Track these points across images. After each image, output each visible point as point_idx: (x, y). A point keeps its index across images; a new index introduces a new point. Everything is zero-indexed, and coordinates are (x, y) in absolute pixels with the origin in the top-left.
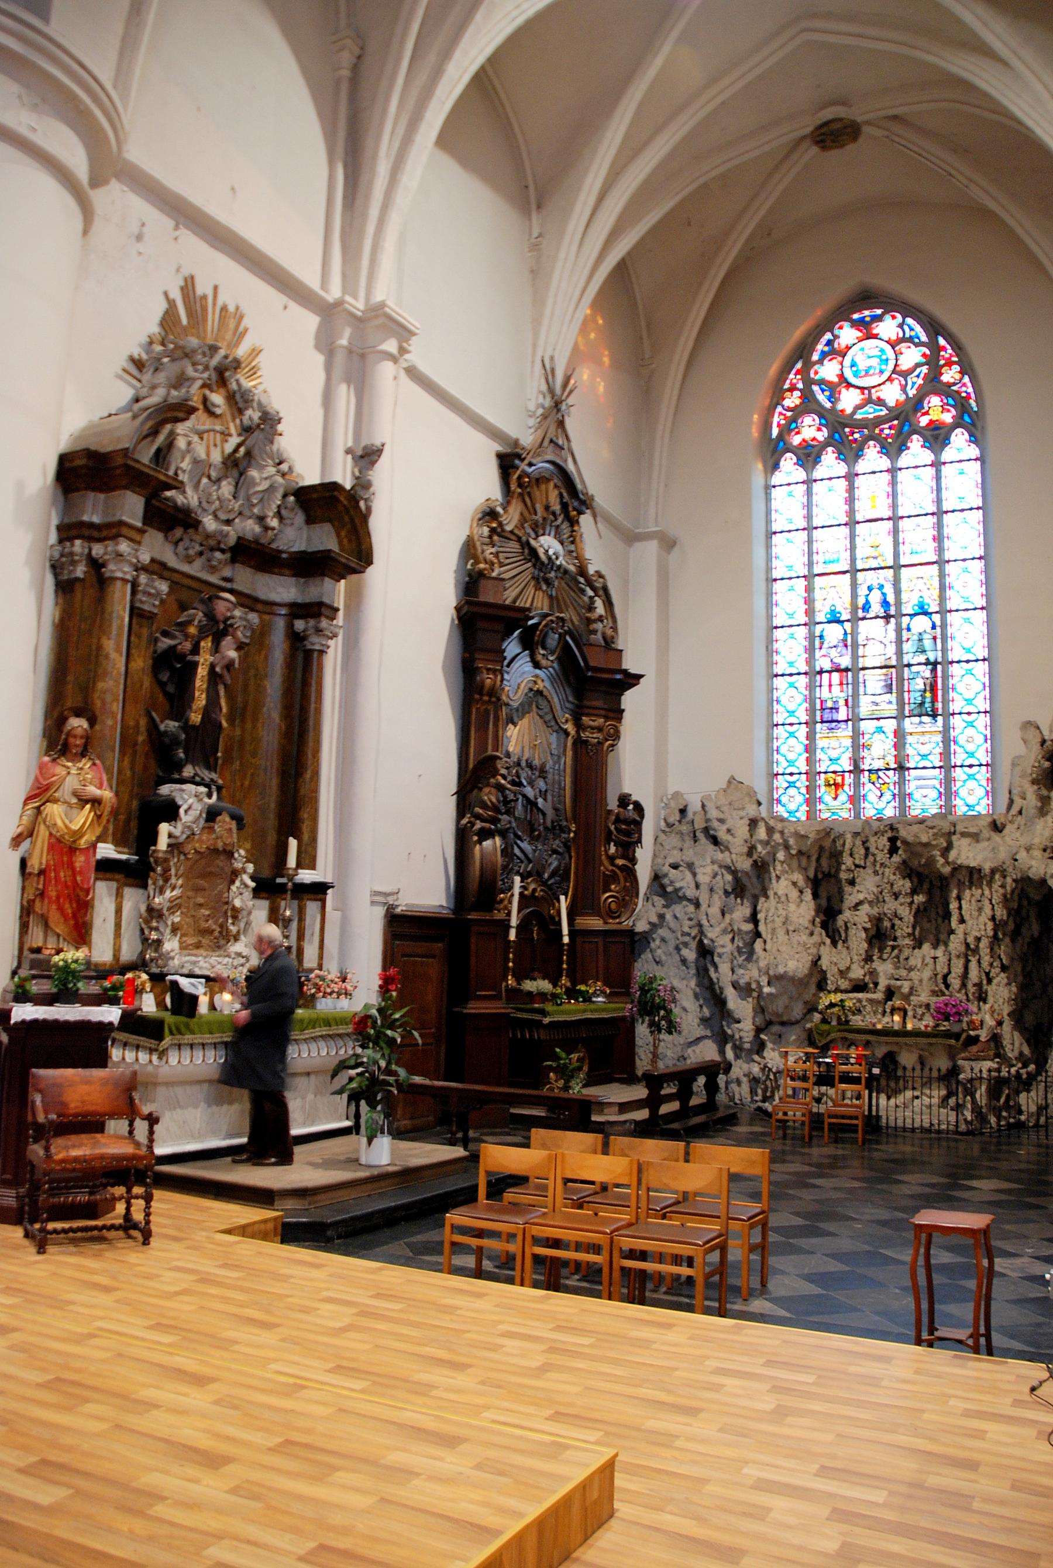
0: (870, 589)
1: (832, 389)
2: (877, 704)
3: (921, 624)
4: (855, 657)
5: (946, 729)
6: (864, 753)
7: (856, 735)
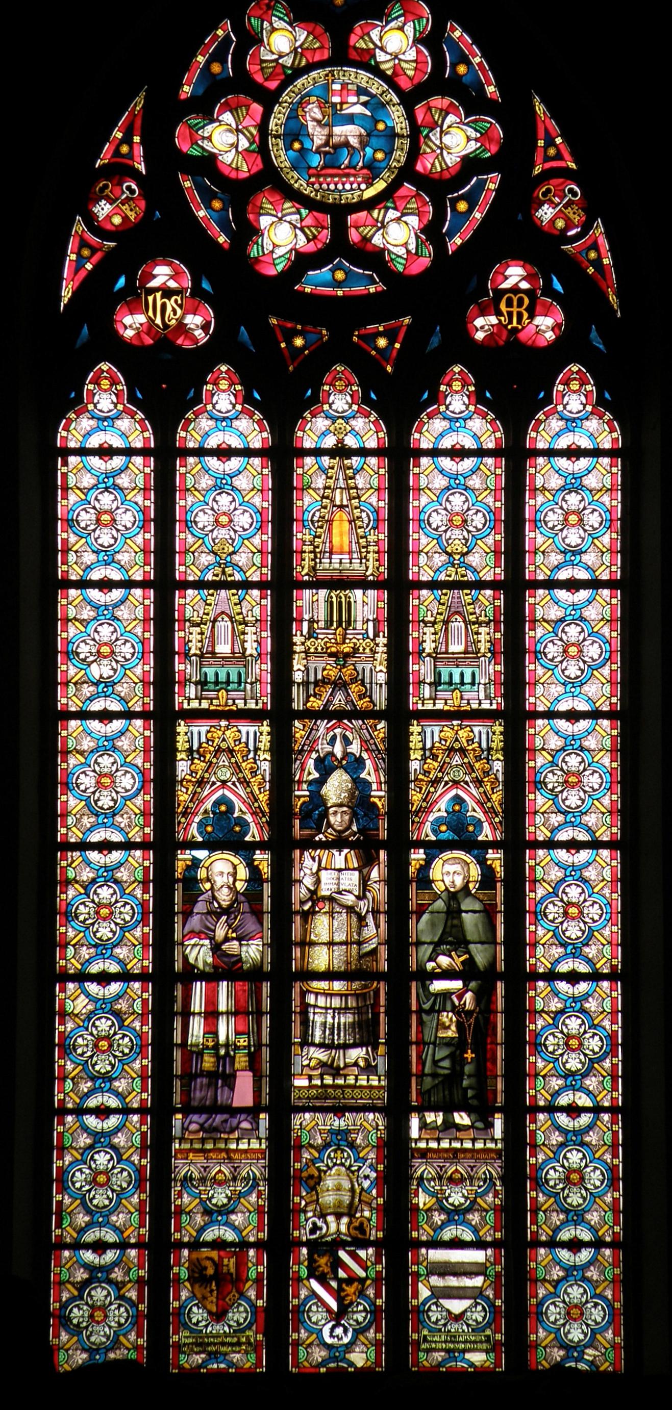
0: (326, 767)
1: (241, 196)
2: (337, 1073)
3: (451, 872)
4: (281, 944)
5: (517, 1143)
6: (299, 1200)
7: (282, 1145)
